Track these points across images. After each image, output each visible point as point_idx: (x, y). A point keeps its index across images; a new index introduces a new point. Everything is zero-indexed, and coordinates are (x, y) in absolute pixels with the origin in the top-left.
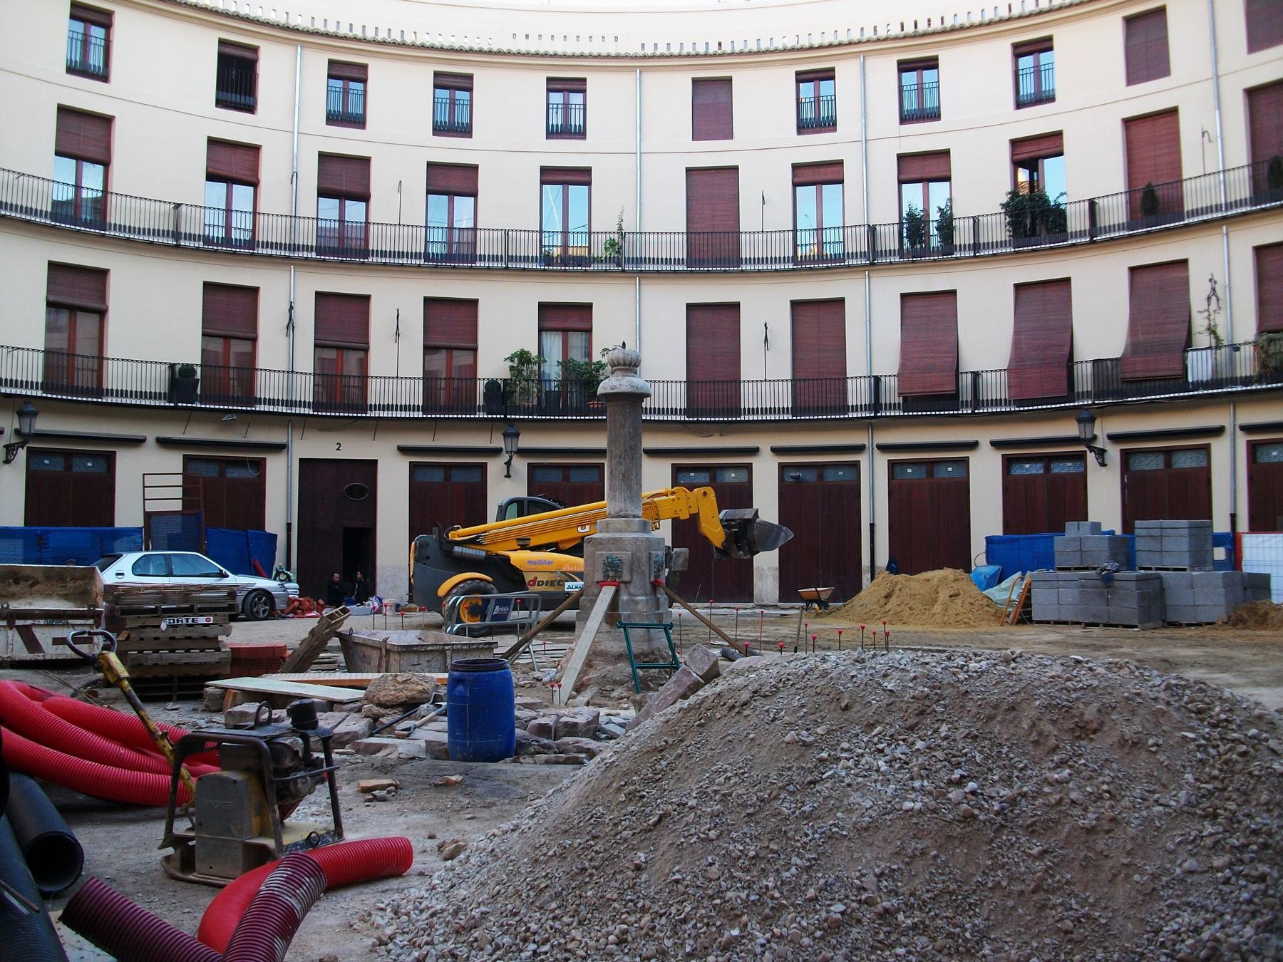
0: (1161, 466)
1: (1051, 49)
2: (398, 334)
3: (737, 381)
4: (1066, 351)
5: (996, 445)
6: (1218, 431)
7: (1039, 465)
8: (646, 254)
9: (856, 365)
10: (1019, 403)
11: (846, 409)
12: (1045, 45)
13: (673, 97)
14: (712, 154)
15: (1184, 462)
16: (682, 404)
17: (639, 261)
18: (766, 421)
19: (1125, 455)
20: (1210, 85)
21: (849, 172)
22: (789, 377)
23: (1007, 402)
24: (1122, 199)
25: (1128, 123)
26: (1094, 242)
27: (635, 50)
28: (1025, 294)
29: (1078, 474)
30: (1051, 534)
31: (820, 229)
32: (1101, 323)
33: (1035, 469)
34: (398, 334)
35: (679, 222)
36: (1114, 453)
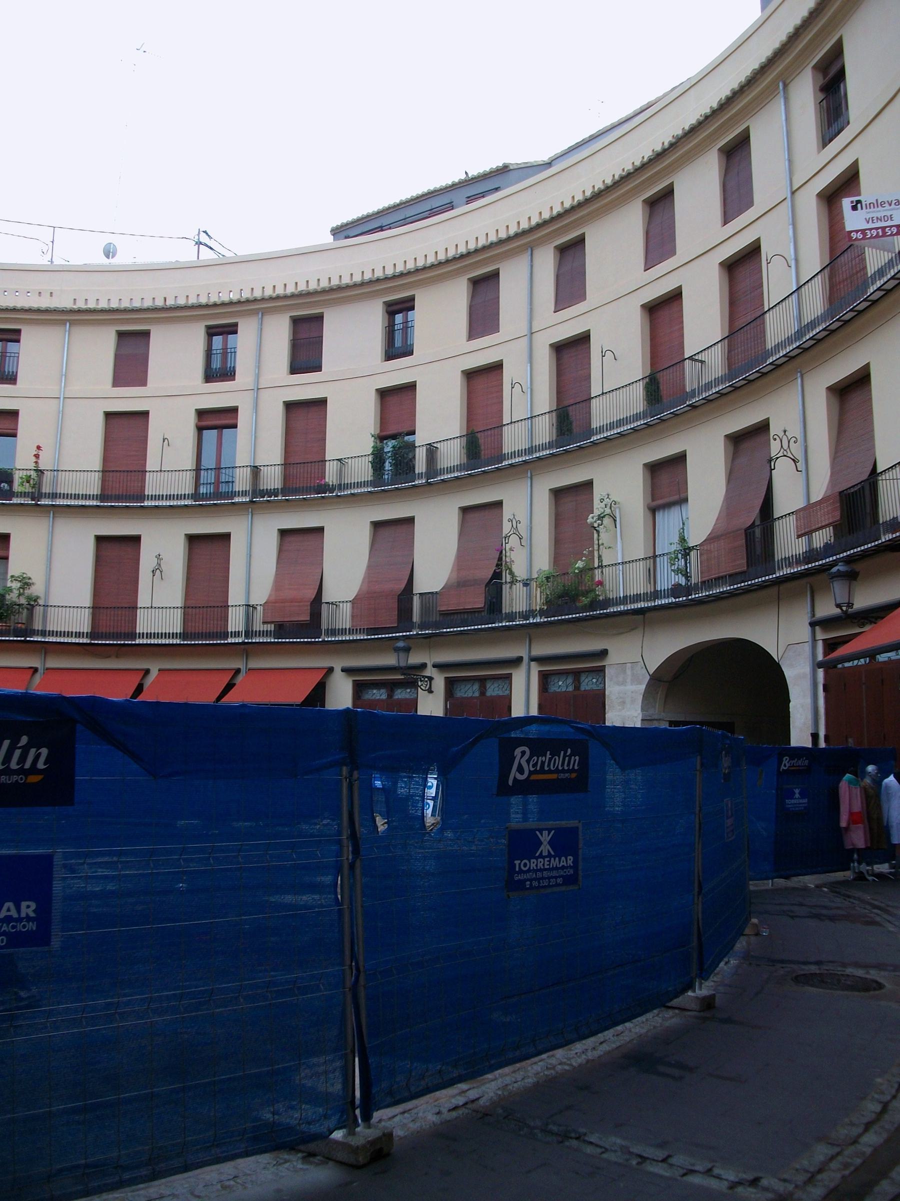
0: (477, 694)
1: (236, 332)
3: (135, 608)
4: (311, 594)
5: (347, 671)
6: (518, 661)
7: (383, 691)
8: (61, 490)
9: (236, 596)
10: (371, 631)
11: (225, 635)
12: (232, 329)
13: (99, 349)
14: (128, 399)
15: (493, 690)
16: (86, 628)
17: (54, 496)
18: (151, 644)
19: (450, 684)
20: (524, 342)
21: (243, 419)
22: (179, 602)
23: (351, 631)
26: (430, 484)
27: (68, 304)
28: (471, 516)
29: (412, 700)
30: (647, 725)
31: (218, 469)
32: (435, 563)
33: (379, 694)
35: (96, 462)
36: (439, 683)
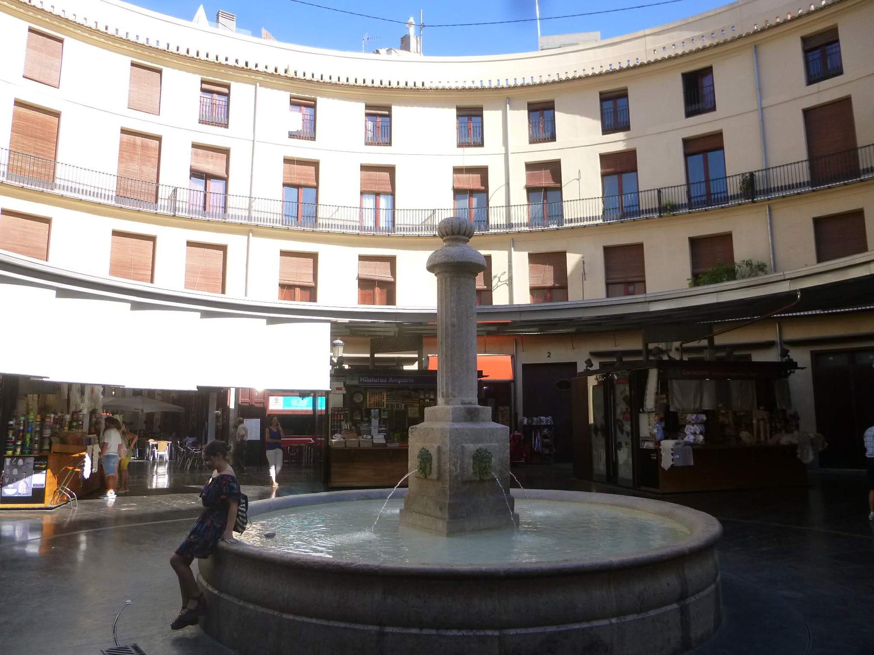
2: (584, 274)
24: (806, 165)
25: (806, 112)
34: (584, 274)
35: (802, 153)
